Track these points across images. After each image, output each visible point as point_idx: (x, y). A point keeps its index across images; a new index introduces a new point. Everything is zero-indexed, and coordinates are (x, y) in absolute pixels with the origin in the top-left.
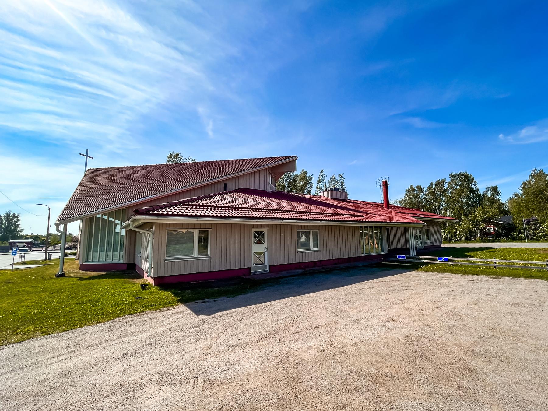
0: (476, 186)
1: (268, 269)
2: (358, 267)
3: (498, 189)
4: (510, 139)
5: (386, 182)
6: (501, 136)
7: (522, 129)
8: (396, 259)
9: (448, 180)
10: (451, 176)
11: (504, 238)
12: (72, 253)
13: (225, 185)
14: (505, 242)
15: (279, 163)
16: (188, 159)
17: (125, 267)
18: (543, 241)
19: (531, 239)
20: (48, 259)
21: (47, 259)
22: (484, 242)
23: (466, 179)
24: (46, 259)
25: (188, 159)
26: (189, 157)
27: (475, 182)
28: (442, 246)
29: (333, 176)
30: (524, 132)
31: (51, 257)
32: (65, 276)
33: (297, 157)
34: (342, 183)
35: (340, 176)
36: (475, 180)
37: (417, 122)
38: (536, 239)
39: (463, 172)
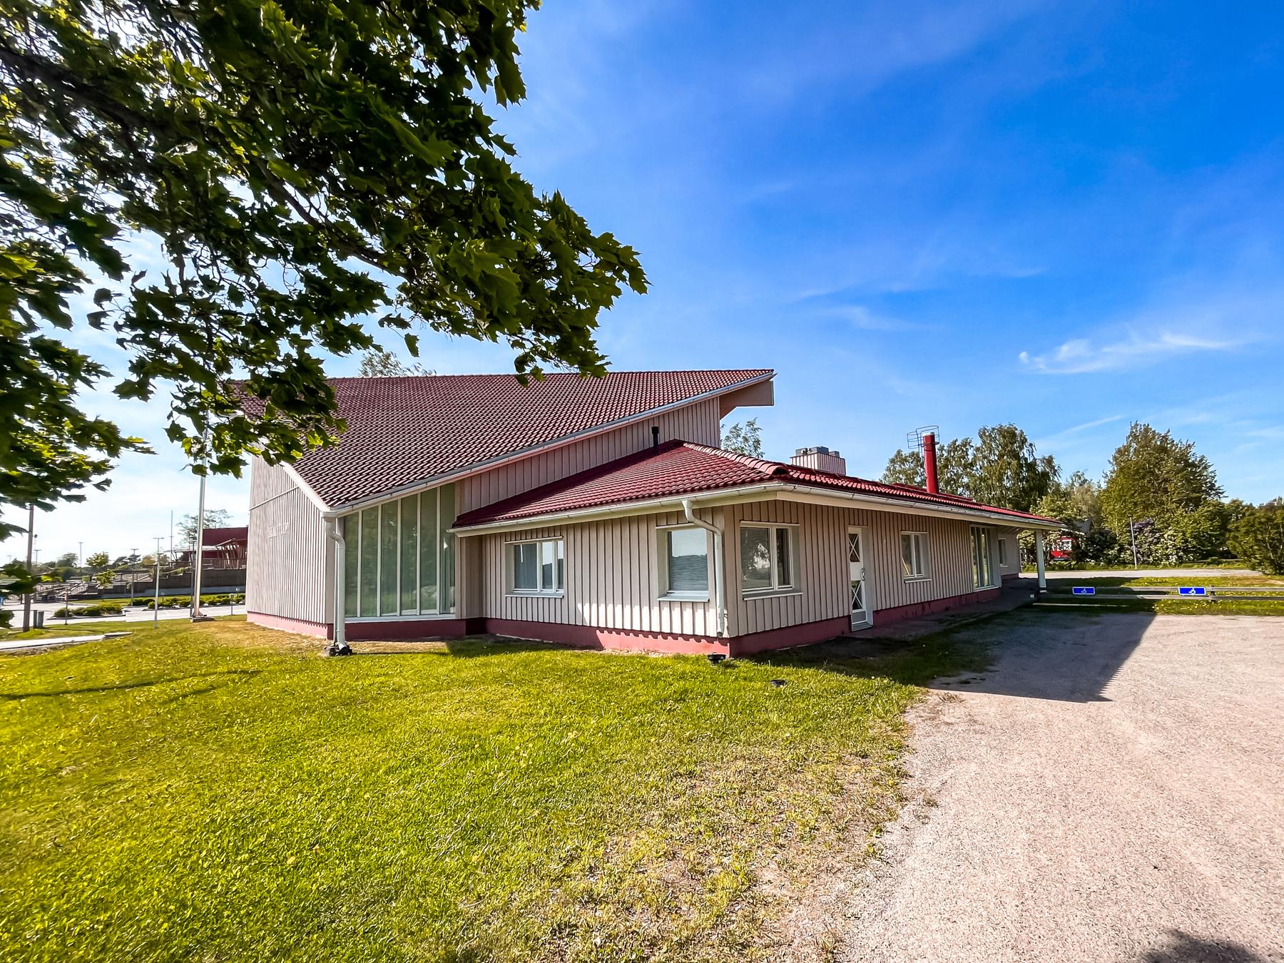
0: (1127, 449)
1: (869, 620)
2: (1005, 614)
3: (1056, 463)
4: (1041, 363)
5: (932, 437)
6: (1023, 355)
7: (1061, 343)
8: (1070, 596)
9: (977, 442)
10: (982, 434)
11: (1093, 562)
12: (81, 609)
13: (656, 431)
14: (1093, 568)
15: (748, 383)
16: (412, 369)
17: (464, 626)
18: (1165, 567)
19: (1144, 562)
20: (35, 627)
21: (31, 624)
22: (1053, 569)
23: (1011, 439)
24: (26, 628)
25: (412, 369)
26: (417, 365)
27: (1031, 445)
28: (1021, 575)
29: (735, 428)
30: (1065, 351)
31: (42, 621)
32: (352, 654)
33: (774, 373)
34: (757, 442)
35: (751, 424)
36: (1029, 441)
37: (859, 315)
38: (1153, 564)
39: (1005, 425)
